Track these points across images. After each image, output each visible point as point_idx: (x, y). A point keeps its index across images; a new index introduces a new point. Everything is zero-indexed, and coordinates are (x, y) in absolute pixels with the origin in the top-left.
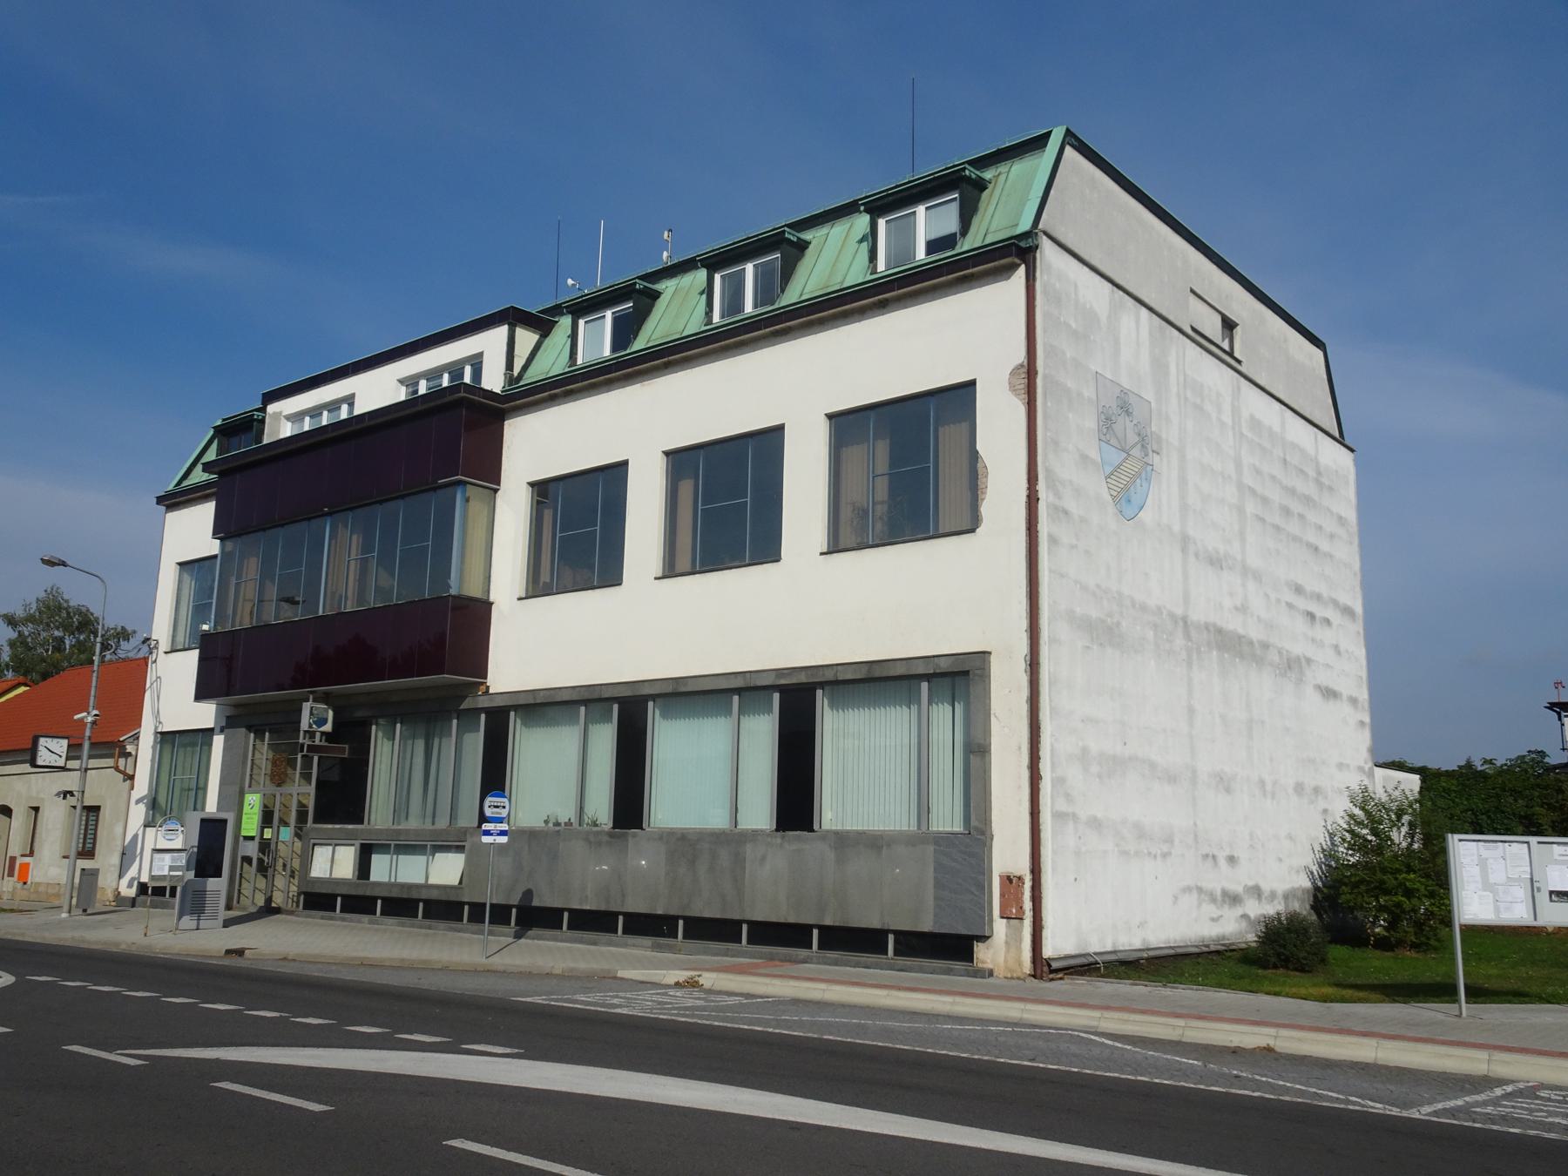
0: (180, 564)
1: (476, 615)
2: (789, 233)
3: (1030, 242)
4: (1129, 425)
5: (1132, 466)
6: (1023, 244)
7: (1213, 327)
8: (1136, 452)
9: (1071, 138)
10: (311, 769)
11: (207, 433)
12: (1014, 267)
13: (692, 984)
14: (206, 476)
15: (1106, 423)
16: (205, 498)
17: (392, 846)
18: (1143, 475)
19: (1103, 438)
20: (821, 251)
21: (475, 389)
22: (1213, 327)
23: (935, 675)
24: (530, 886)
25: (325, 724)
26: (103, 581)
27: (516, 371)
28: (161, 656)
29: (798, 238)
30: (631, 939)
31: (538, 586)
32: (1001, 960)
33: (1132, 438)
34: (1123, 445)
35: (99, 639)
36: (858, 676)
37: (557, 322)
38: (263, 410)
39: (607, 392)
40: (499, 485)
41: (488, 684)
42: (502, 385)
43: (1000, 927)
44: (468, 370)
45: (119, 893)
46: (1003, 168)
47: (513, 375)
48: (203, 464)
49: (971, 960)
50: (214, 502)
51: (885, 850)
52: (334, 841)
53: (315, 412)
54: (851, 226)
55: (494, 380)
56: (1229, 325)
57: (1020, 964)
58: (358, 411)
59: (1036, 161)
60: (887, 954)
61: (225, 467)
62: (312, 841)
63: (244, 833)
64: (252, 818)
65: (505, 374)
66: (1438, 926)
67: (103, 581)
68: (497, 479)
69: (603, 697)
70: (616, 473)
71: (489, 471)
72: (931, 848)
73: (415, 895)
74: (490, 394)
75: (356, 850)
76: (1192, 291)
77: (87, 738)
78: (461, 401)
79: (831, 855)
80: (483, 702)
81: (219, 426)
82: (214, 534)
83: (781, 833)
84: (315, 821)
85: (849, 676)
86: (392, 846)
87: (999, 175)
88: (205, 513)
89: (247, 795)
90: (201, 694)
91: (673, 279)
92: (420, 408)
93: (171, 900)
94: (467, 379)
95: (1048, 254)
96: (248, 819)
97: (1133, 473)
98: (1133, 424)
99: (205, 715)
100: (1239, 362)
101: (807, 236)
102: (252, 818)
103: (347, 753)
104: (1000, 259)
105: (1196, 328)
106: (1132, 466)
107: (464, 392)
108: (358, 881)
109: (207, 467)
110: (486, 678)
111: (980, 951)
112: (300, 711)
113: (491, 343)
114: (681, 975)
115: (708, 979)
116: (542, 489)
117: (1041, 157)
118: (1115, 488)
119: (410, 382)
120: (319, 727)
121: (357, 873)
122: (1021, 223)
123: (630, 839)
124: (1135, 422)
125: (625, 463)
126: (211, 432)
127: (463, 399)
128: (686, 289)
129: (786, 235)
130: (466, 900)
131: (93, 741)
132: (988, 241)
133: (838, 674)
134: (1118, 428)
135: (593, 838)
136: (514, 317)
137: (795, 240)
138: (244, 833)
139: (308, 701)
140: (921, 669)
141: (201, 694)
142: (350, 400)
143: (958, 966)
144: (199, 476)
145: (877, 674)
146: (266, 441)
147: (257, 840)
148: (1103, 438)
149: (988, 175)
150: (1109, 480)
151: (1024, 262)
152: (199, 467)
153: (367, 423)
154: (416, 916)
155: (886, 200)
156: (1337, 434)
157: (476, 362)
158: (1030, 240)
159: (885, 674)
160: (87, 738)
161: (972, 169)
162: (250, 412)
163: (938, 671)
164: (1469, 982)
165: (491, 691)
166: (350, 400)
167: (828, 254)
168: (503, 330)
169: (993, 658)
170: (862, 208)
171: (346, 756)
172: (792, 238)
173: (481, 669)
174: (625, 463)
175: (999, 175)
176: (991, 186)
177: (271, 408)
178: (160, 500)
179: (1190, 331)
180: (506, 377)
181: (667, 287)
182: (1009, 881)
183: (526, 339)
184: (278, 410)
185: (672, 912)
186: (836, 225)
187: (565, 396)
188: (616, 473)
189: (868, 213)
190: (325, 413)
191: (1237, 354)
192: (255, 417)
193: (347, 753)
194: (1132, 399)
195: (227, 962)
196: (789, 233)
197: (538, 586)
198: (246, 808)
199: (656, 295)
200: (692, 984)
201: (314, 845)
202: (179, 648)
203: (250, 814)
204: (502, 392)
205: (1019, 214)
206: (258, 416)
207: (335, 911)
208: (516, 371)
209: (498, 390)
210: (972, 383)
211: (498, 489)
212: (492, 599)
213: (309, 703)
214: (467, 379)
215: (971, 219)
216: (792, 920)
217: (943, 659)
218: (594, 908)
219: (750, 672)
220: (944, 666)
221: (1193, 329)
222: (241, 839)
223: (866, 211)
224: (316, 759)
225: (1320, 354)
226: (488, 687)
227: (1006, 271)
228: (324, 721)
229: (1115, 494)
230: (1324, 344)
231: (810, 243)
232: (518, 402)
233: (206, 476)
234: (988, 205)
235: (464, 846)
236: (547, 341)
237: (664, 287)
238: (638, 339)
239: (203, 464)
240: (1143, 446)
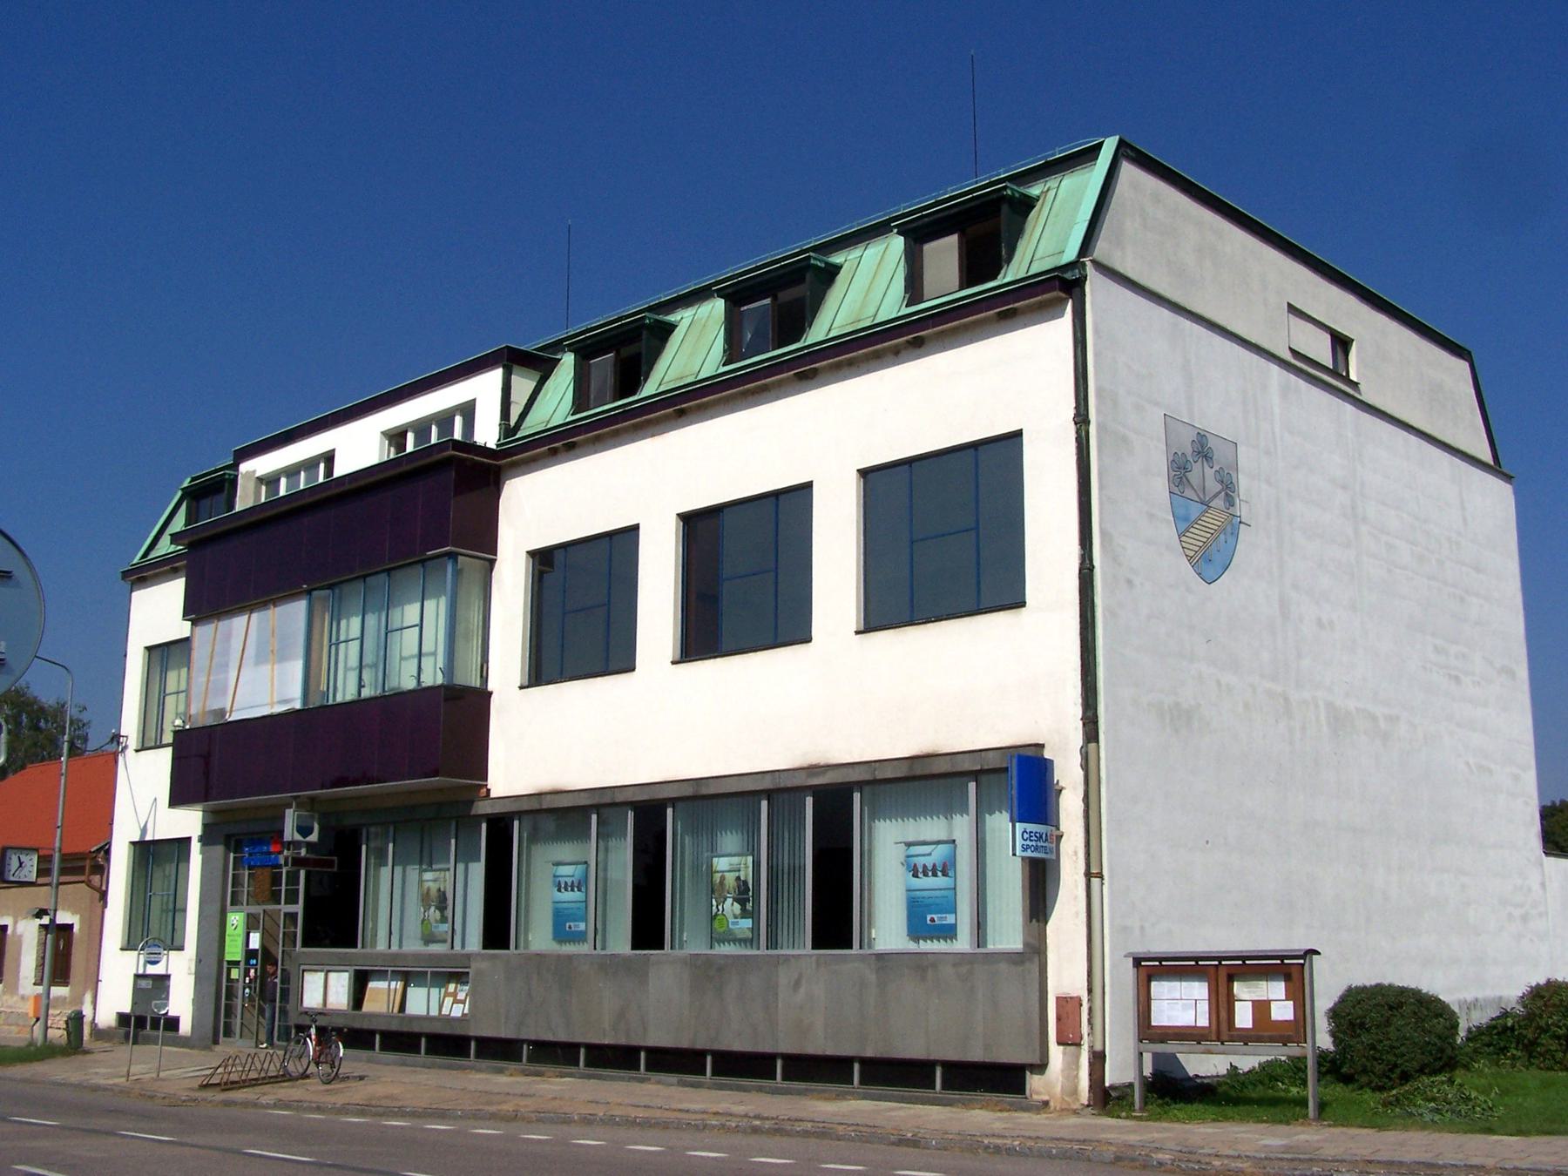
1: (205, 839)
2: (815, 259)
3: (1076, 274)
4: (1209, 472)
5: (1213, 519)
6: (1068, 276)
7: (1321, 349)
8: (1219, 503)
9: (1126, 151)
10: (298, 884)
11: (176, 493)
12: (1063, 302)
14: (173, 548)
15: (1179, 471)
16: (173, 573)
17: (389, 972)
18: (1229, 529)
19: (1176, 490)
20: (853, 277)
21: (468, 446)
22: (1321, 349)
23: (982, 772)
25: (311, 833)
26: (66, 668)
27: (513, 422)
28: (130, 752)
29: (826, 263)
31: (540, 672)
33: (1213, 486)
34: (1202, 497)
35: (66, 738)
36: (899, 775)
37: (560, 360)
38: (235, 466)
40: (496, 555)
41: (489, 787)
42: (497, 438)
43: (1056, 1053)
44: (458, 421)
45: (96, 1025)
46: (1052, 182)
47: (510, 425)
48: (171, 535)
50: (184, 579)
51: (930, 972)
52: (327, 967)
53: (292, 472)
54: (886, 248)
55: (487, 433)
56: (1341, 343)
57: (1075, 1092)
58: (339, 472)
59: (1087, 175)
60: (934, 1088)
61: (196, 537)
62: (302, 967)
63: (228, 957)
64: (236, 941)
65: (500, 425)
66: (1414, 1074)
67: (66, 668)
68: (493, 549)
69: (617, 801)
70: (630, 534)
71: (484, 540)
73: (416, 1029)
74: (484, 450)
75: (350, 975)
76: (1292, 309)
77: (57, 850)
78: (449, 461)
79: (872, 977)
80: (482, 808)
81: (185, 488)
82: (184, 616)
84: (305, 944)
85: (889, 775)
86: (389, 972)
87: (1048, 190)
88: (173, 591)
89: (229, 915)
90: (179, 797)
91: (690, 309)
92: (406, 468)
93: (154, 1033)
94: (458, 435)
95: (1096, 286)
96: (232, 941)
97: (1216, 528)
98: (1214, 470)
99: (188, 822)
100: (1355, 385)
101: (837, 259)
102: (236, 941)
103: (336, 866)
104: (1043, 294)
105: (1296, 349)
106: (1213, 519)
107: (453, 450)
108: (354, 1012)
109: (175, 538)
110: (486, 780)
111: (1034, 1082)
112: (283, 817)
113: (484, 389)
116: (544, 560)
117: (1092, 171)
118: (1191, 547)
119: (396, 437)
120: (305, 837)
121: (351, 1004)
122: (1067, 251)
124: (1216, 468)
125: (635, 529)
126: (179, 494)
127: (452, 457)
128: (703, 321)
129: (812, 261)
130: (471, 1034)
131: (63, 852)
132: (1034, 270)
133: (876, 773)
134: (1194, 476)
135: (610, 966)
136: (511, 359)
137: (823, 265)
138: (228, 957)
139: (291, 807)
140: (968, 765)
141: (179, 797)
142: (329, 458)
143: (1009, 1098)
144: (165, 547)
145: (919, 772)
146: (239, 507)
148: (1176, 490)
149: (1035, 191)
150: (1184, 539)
151: (1071, 298)
152: (166, 539)
153: (347, 487)
154: (419, 1052)
155: (920, 223)
156: (1486, 456)
157: (468, 410)
158: (1077, 271)
159: (927, 771)
160: (57, 850)
161: (1015, 187)
162: (221, 469)
163: (986, 767)
165: (493, 795)
166: (329, 458)
167: (861, 281)
168: (495, 377)
170: (895, 231)
171: (335, 869)
172: (819, 264)
173: (483, 773)
174: (635, 529)
175: (1048, 190)
176: (1039, 204)
177: (245, 467)
178: (125, 574)
179: (1288, 357)
180: (500, 429)
181: (683, 318)
182: (1068, 1005)
183: (523, 385)
184: (252, 469)
185: (699, 1045)
186: (870, 246)
188: (630, 534)
189: (901, 235)
190: (283, 481)
191: (1353, 377)
192: (227, 477)
193: (336, 866)
194: (1212, 443)
196: (815, 259)
197: (540, 672)
198: (229, 930)
199: (670, 328)
201: (304, 971)
202: (149, 745)
203: (233, 935)
204: (498, 446)
205: (1066, 240)
206: (230, 475)
208: (513, 422)
209: (492, 445)
210: (1018, 434)
211: (496, 560)
212: (490, 688)
213: (292, 810)
214: (458, 435)
215: (1017, 242)
216: (830, 1052)
217: (991, 753)
218: (612, 1042)
219: (778, 771)
221: (1294, 352)
223: (898, 233)
224: (302, 873)
225: (1462, 366)
226: (489, 791)
227: (1047, 311)
228: (310, 831)
229: (1192, 553)
230: (1469, 353)
231: (841, 267)
232: (515, 458)
233: (173, 548)
234: (1035, 226)
235: (468, 973)
236: (550, 384)
237: (679, 318)
238: (649, 380)
239: (171, 535)
240: (1227, 494)
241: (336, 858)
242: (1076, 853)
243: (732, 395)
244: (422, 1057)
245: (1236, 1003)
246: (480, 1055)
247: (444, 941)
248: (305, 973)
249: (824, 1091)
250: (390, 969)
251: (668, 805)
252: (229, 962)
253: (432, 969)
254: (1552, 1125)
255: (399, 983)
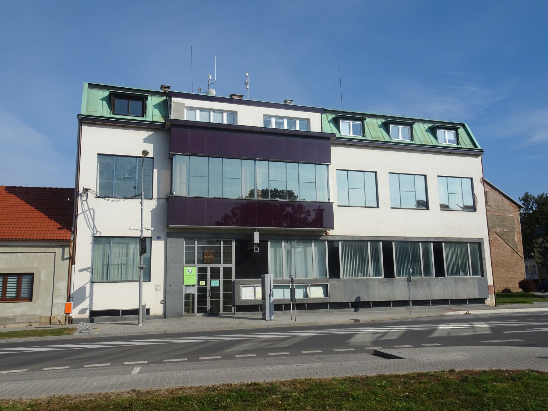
0: (98, 154)
13: (467, 313)
17: (310, 285)
24: (359, 296)
30: (332, 310)
32: (490, 303)
39: (367, 149)
49: (485, 303)
51: (466, 281)
57: (493, 303)
72: (476, 280)
73: (280, 303)
83: (436, 278)
86: (310, 285)
114: (465, 312)
115: (470, 312)
123: (394, 280)
147: (196, 286)
155: (441, 126)
164: (89, 322)
169: (484, 239)
171: (255, 252)
185: (257, 304)
187: (350, 145)
195: (372, 322)
200: (467, 313)
207: (119, 315)
220: (449, 240)
222: (184, 286)
241: (255, 252)
242: (489, 259)
243: (134, 126)
244: (329, 310)
245: (302, 289)
246: (331, 308)
247: (126, 278)
248: (253, 287)
249: (475, 307)
250: (310, 284)
251: (233, 240)
252: (186, 286)
253: (311, 284)
254: (5, 320)
255: (27, 295)
